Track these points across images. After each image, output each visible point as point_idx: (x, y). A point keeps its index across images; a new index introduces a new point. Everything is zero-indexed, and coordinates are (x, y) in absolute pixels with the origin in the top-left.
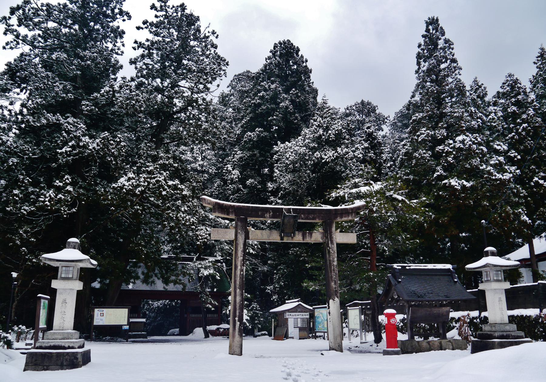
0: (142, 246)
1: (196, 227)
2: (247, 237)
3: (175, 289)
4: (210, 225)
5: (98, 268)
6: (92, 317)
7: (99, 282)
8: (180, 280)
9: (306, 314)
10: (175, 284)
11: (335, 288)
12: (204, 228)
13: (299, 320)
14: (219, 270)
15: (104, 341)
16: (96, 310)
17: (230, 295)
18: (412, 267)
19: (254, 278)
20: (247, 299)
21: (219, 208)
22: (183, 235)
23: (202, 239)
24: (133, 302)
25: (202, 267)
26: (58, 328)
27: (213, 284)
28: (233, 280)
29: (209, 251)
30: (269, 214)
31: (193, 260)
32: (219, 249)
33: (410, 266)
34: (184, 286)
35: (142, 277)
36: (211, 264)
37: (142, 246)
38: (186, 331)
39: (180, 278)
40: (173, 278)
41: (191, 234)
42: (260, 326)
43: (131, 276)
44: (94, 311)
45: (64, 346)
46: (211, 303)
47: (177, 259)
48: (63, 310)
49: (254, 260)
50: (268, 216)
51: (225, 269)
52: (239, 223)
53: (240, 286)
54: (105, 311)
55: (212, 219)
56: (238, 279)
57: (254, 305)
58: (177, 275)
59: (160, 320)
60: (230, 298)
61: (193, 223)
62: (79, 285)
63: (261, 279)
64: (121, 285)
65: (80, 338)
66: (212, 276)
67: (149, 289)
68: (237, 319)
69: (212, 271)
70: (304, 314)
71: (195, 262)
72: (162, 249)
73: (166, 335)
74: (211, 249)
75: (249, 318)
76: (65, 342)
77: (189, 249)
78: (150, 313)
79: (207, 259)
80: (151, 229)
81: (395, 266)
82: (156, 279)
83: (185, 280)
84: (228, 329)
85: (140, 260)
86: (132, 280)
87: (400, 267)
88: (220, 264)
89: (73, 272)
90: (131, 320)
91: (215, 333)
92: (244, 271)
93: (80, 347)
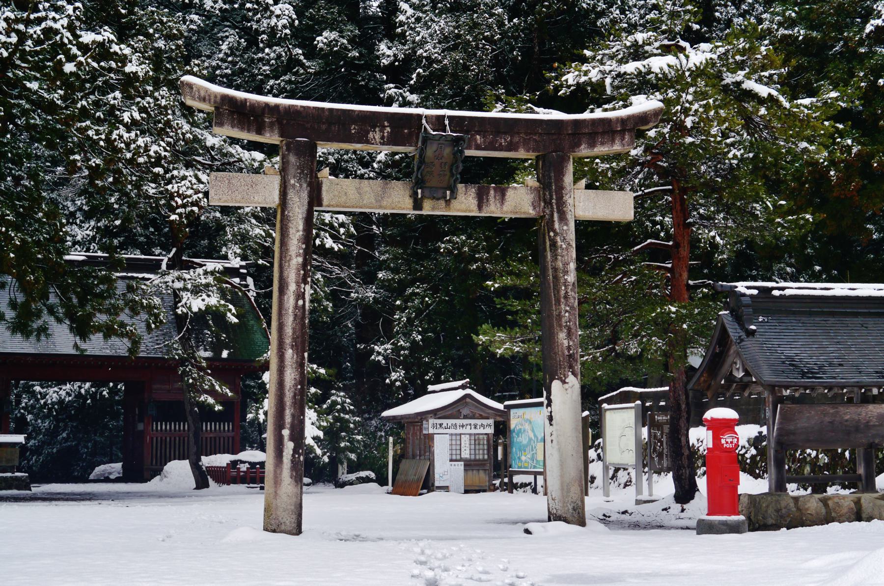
0: (9, 224)
1: (167, 171)
2: (315, 198)
3: (108, 352)
8: (122, 325)
9: (485, 422)
10: (107, 336)
11: (569, 348)
12: (189, 173)
13: (465, 440)
14: (234, 297)
18: (788, 292)
19: (337, 321)
20: (316, 381)
21: (232, 113)
22: (127, 195)
23: (184, 206)
25: (185, 289)
27: (218, 337)
29: (205, 242)
30: (382, 131)
32: (234, 235)
33: (783, 289)
34: (136, 342)
36: (210, 279)
38: (140, 469)
39: (123, 317)
40: (101, 318)
41: (151, 192)
42: (353, 456)
47: (113, 264)
49: (336, 270)
50: (378, 136)
52: (292, 159)
55: (213, 148)
56: (289, 320)
57: (338, 397)
58: (114, 311)
59: (65, 440)
60: (266, 377)
63: (357, 325)
66: (217, 315)
68: (286, 433)
69: (213, 300)
70: (479, 422)
71: (164, 274)
72: (66, 233)
73: (86, 481)
77: (146, 236)
79: (201, 266)
80: (33, 175)
81: (741, 287)
82: (51, 320)
83: (137, 324)
87: (755, 292)
88: (237, 280)
92: (307, 297)
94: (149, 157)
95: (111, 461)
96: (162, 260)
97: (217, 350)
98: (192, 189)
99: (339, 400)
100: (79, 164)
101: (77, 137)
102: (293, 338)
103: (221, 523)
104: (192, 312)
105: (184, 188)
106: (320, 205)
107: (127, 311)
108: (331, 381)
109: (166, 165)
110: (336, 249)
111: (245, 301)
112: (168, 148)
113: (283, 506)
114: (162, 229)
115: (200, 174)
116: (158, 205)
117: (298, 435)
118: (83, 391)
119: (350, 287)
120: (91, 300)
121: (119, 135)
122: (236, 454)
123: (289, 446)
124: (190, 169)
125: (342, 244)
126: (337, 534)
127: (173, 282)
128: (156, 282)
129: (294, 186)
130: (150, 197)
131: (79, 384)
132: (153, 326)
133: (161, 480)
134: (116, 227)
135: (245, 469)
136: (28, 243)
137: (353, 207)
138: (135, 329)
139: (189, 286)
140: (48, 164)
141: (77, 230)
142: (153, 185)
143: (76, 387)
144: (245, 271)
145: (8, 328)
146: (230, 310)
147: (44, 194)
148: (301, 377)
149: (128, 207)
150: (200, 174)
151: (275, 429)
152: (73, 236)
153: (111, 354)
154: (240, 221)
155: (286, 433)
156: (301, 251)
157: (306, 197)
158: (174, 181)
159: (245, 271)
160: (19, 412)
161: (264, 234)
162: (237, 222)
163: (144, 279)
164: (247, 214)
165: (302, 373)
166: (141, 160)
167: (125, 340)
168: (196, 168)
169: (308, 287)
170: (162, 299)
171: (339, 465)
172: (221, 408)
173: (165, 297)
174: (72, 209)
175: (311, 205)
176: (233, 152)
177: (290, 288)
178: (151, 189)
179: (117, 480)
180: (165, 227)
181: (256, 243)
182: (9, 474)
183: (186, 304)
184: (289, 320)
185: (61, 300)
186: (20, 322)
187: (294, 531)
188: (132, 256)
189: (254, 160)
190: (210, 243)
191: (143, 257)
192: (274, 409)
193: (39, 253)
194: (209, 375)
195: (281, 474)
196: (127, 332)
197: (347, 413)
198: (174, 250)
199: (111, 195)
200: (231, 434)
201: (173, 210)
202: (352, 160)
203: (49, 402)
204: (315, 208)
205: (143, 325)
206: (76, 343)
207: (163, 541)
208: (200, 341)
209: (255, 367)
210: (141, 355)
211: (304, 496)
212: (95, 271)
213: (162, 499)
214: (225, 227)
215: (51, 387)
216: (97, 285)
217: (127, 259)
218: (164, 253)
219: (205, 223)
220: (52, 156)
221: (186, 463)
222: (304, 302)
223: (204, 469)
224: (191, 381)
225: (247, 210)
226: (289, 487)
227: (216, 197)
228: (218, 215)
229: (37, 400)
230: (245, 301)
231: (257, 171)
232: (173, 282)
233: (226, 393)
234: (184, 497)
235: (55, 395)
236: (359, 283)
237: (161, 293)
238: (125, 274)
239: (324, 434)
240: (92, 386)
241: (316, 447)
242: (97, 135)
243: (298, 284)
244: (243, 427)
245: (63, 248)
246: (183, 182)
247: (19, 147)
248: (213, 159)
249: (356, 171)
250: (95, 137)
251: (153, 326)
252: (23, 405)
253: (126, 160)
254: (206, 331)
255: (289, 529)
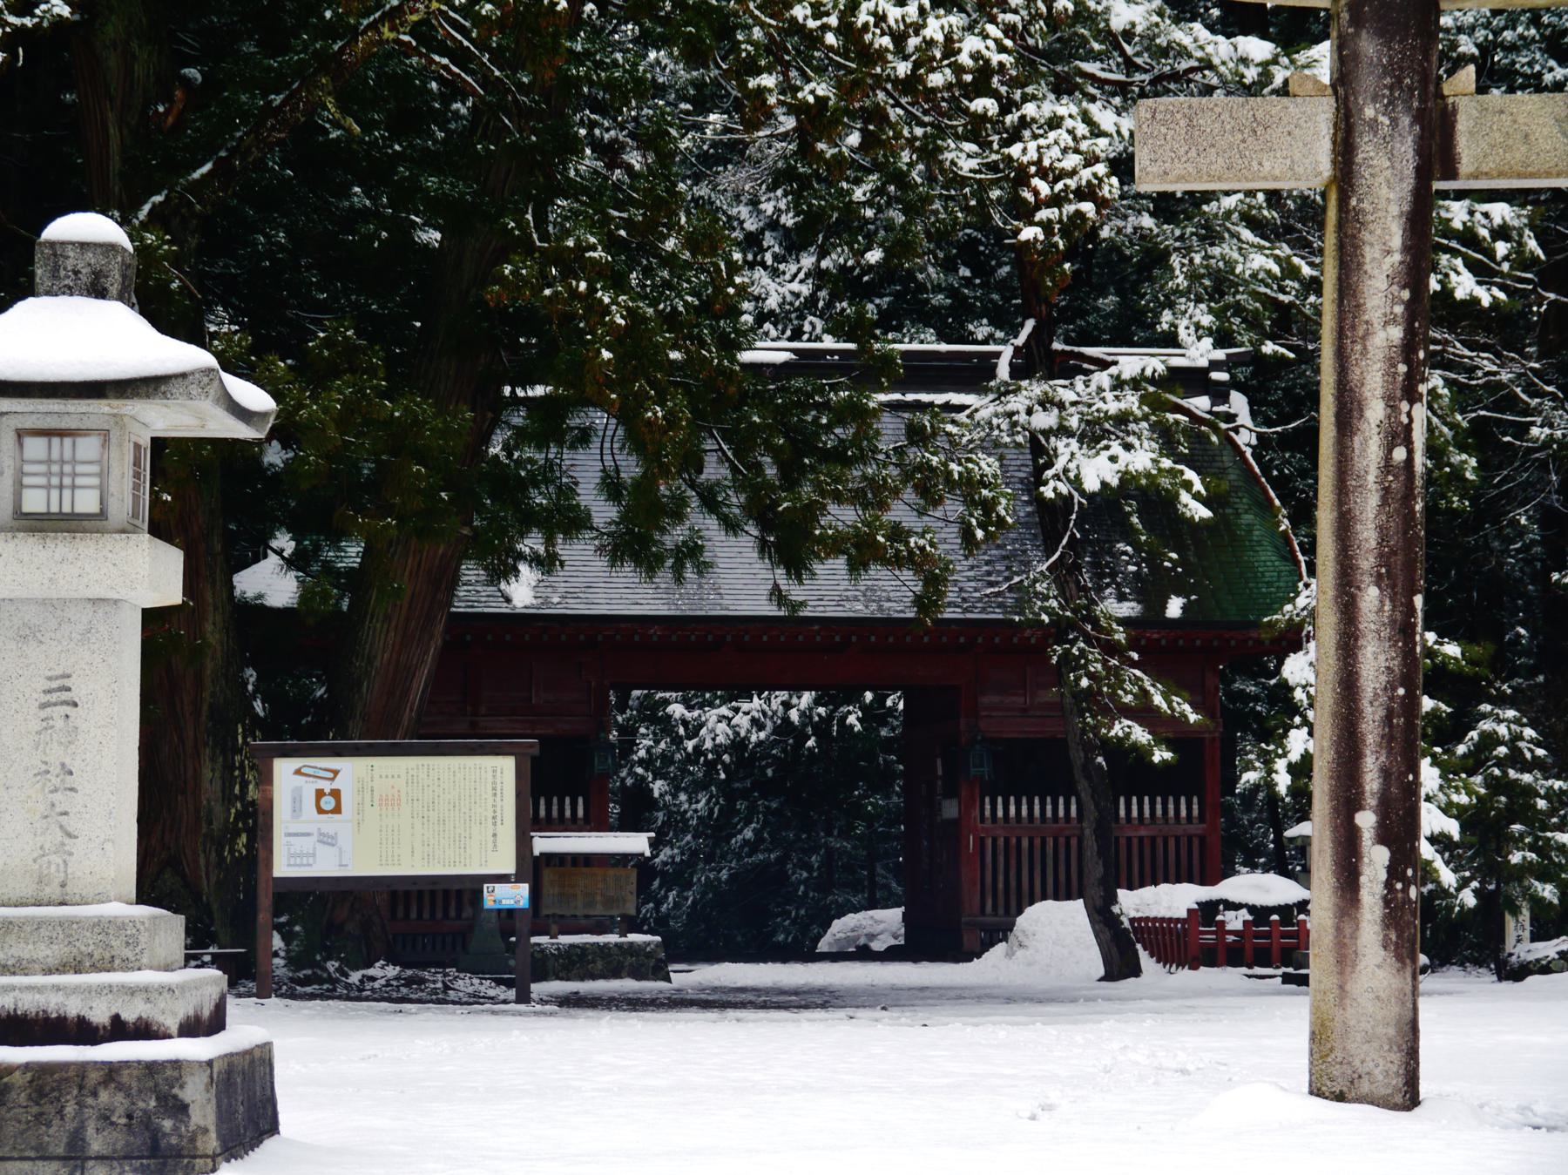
0: (596, 272)
1: (1007, 106)
2: (1436, 154)
3: (859, 609)
4: (1122, 89)
5: (275, 456)
6: (257, 822)
7: (292, 563)
8: (898, 533)
10: (857, 566)
12: (1066, 108)
14: (1198, 446)
15: (356, 994)
16: (283, 768)
17: (1296, 646)
19: (1489, 508)
20: (1440, 679)
22: (901, 179)
23: (1056, 201)
24: (552, 706)
25: (1063, 431)
26: (27, 889)
27: (1154, 559)
28: (1325, 517)
29: (1109, 302)
31: (991, 372)
32: (1193, 276)
34: (934, 579)
35: (604, 512)
36: (1131, 401)
37: (596, 272)
38: (951, 928)
39: (900, 512)
40: (842, 516)
41: (967, 165)
42: (1548, 891)
43: (518, 512)
44: (266, 778)
45: (82, 1021)
46: (1144, 712)
47: (870, 370)
48: (56, 755)
49: (1486, 363)
51: (1245, 439)
52: (1369, 47)
53: (1384, 558)
54: (352, 772)
55: (1128, 34)
56: (1369, 506)
57: (1499, 722)
58: (874, 496)
59: (753, 846)
60: (1296, 669)
61: (984, 70)
62: (155, 574)
63: (1546, 517)
64: (454, 581)
65: (190, 960)
66: (1150, 497)
67: (663, 610)
68: (1366, 820)
69: (1142, 458)
71: (1003, 393)
72: (743, 291)
73: (809, 955)
74: (1129, 291)
75: (1453, 828)
76: (88, 990)
77: (951, 292)
78: (676, 790)
79: (1103, 365)
80: (652, 139)
82: (710, 526)
83: (937, 529)
84: (1290, 912)
85: (583, 386)
86: (533, 543)
88: (1201, 404)
89: (103, 475)
90: (544, 844)
91: (1188, 944)
92: (1419, 437)
93: (193, 1028)
94: (958, 69)
95: (873, 904)
96: (998, 355)
97: (1153, 597)
98: (1077, 151)
99: (1502, 730)
100: (772, 100)
101: (763, 25)
102: (1381, 555)
103: (1184, 1072)
104: (1082, 493)
105: (1055, 152)
106: (1452, 174)
107: (909, 494)
108: (1476, 679)
109: (1003, 90)
110: (1486, 301)
111: (1227, 459)
112: (1009, 43)
113: (1364, 1025)
114: (994, 270)
115: (1094, 109)
116: (983, 203)
117: (1399, 829)
118: (794, 715)
119: (1528, 411)
120: (812, 468)
121: (875, 14)
122: (1212, 881)
123: (1376, 859)
124: (1065, 100)
125: (1502, 287)
126: (1523, 1109)
127: (1029, 412)
128: (984, 414)
129: (1373, 124)
130: (963, 181)
131: (783, 695)
132: (980, 534)
133: (1010, 955)
134: (870, 268)
135: (1238, 926)
136: (645, 319)
137: (1548, 175)
138: (932, 544)
139: (1074, 422)
140: (685, 106)
141: (766, 280)
142: (970, 147)
143: (776, 704)
144: (1222, 376)
145: (600, 549)
146: (1188, 485)
147: (682, 187)
148: (1404, 664)
149: (904, 212)
150: (1094, 109)
151: (1336, 811)
152: (757, 299)
153: (866, 613)
154: (1211, 236)
155: (1366, 820)
156: (1399, 309)
157: (1411, 154)
158: (1027, 134)
159: (1222, 376)
160: (631, 773)
161: (1276, 269)
162: (1202, 239)
163: (947, 407)
164: (1228, 214)
165: (1408, 654)
166: (936, 80)
167: (907, 574)
168: (1085, 94)
169: (1420, 412)
170: (1001, 458)
171: (1509, 918)
172: (1168, 755)
173: (1011, 454)
174: (751, 225)
175: (1423, 175)
176: (1187, 41)
177: (1368, 414)
178: (964, 158)
179: (892, 955)
180: (1000, 265)
181: (1256, 295)
182: (613, 938)
183: (1066, 471)
184: (1369, 506)
185: (734, 470)
186: (630, 532)
187: (1398, 1099)
188: (915, 346)
189: (1244, 61)
190: (1125, 304)
191: (944, 347)
192: (1329, 755)
193: (675, 347)
194: (1134, 665)
195: (1354, 937)
196: (910, 552)
197: (1526, 767)
198: (1030, 324)
199: (858, 182)
200: (1197, 828)
201: (1025, 213)
202: (1526, 42)
203: (708, 745)
204: (1438, 185)
205: (952, 533)
206: (776, 587)
207: (1033, 1118)
208: (1105, 573)
209: (1259, 642)
210: (949, 614)
211: (1423, 1003)
212: (820, 390)
213: (1012, 1006)
214: (1166, 254)
215: (712, 705)
216: (828, 428)
217: (906, 355)
218: (999, 334)
219: (1113, 247)
220: (698, 85)
221: (1077, 907)
222: (1410, 452)
223: (1127, 924)
224: (1085, 682)
225: (1229, 202)
226: (1381, 973)
227: (1154, 169)
228: (1147, 221)
229: (677, 741)
230: (1227, 459)
231: (1252, 90)
232: (1029, 412)
233: (1183, 714)
234: (1074, 1000)
235: (722, 726)
236: (1554, 397)
237: (997, 444)
238: (897, 396)
239: (1463, 829)
240: (817, 702)
241: (1439, 864)
242: (816, 16)
243: (1392, 407)
244: (1228, 810)
245: (736, 330)
246: (1052, 135)
247: (615, 63)
248: (1130, 66)
249: (1539, 75)
250: (812, 24)
251: (980, 534)
252: (642, 753)
253: (896, 81)
254: (1121, 546)
255: (1384, 1091)
